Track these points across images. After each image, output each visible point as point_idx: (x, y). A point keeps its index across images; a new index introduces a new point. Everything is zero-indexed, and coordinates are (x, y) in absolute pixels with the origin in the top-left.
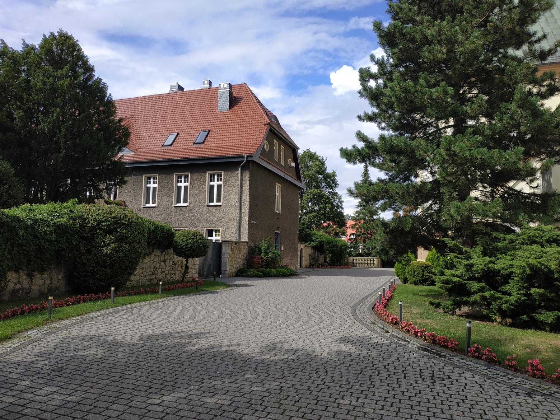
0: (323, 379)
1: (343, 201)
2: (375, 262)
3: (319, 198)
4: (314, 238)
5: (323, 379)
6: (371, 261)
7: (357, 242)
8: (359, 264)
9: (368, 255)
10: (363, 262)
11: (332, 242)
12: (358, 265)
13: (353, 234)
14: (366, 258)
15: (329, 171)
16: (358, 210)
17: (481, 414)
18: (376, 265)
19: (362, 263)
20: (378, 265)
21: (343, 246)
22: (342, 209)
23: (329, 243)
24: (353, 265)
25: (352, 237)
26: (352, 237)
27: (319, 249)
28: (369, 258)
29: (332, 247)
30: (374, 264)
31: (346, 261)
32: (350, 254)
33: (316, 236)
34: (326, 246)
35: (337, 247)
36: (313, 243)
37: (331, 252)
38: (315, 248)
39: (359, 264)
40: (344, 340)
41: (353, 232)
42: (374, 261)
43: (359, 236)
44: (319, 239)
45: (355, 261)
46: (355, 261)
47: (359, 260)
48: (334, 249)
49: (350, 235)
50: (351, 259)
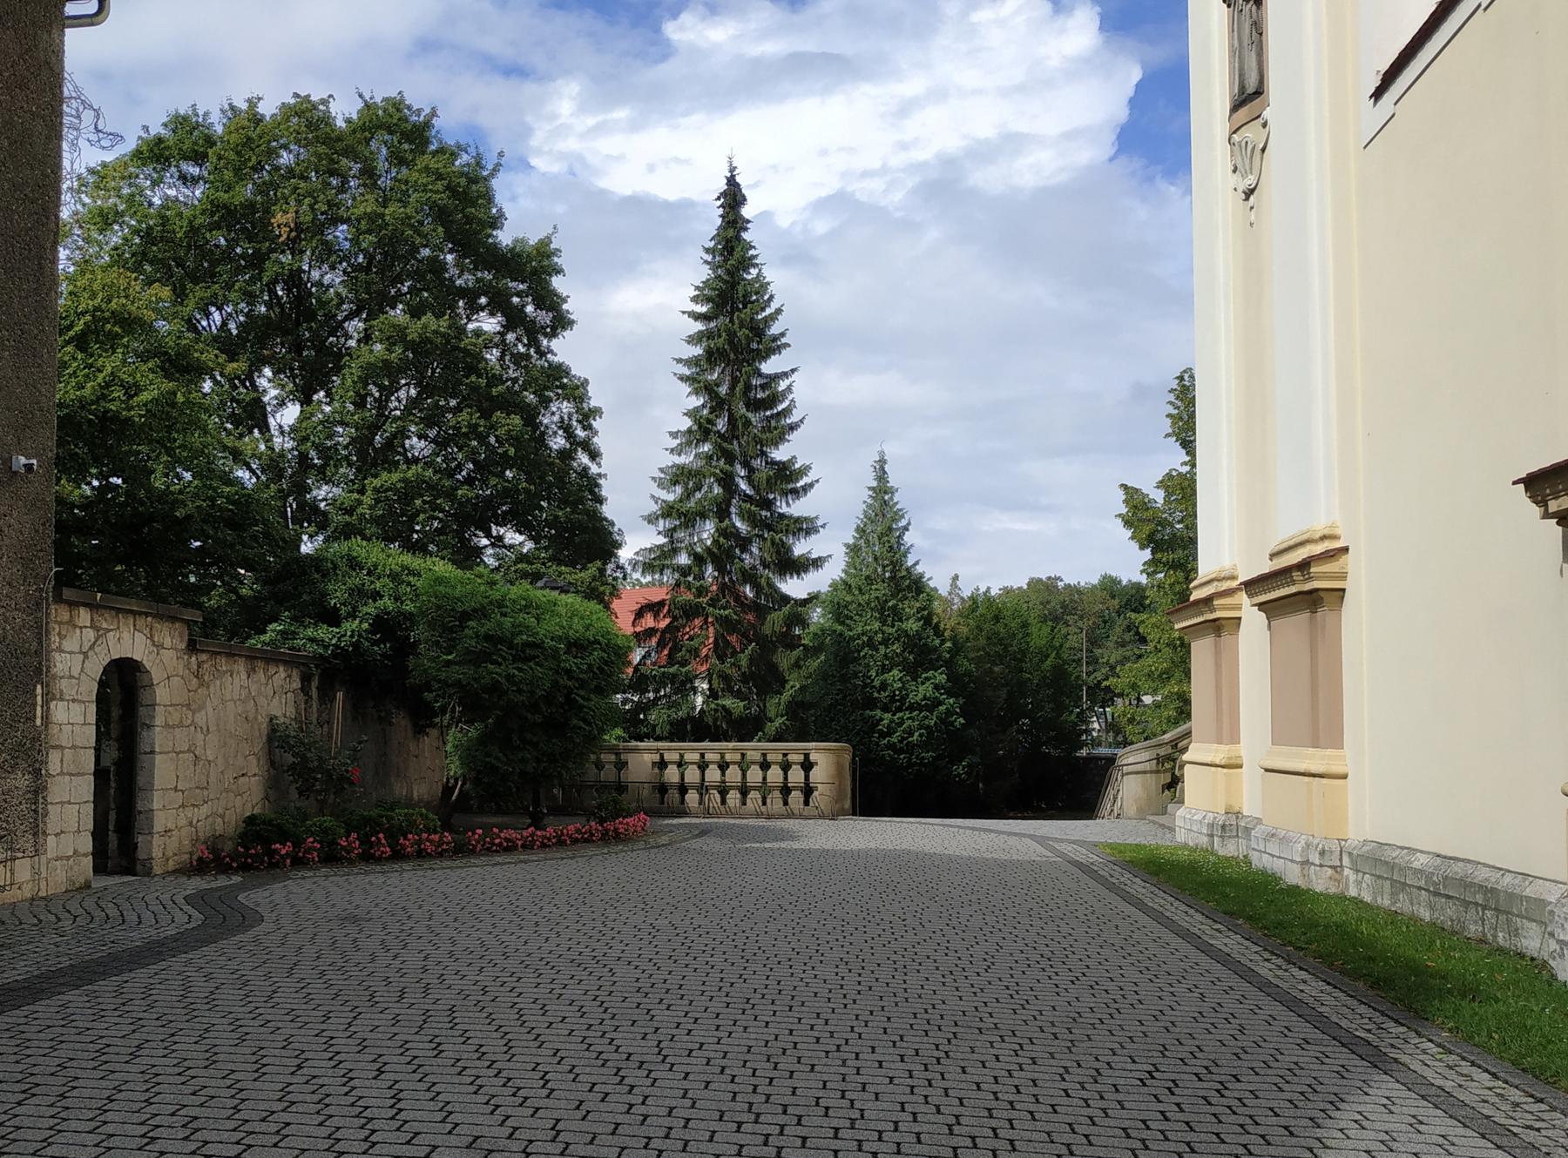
0: (620, 1083)
1: (596, 412)
2: (817, 775)
3: (447, 367)
4: (337, 594)
5: (620, 1083)
6: (765, 766)
7: (676, 648)
8: (702, 788)
9: (745, 728)
10: (733, 774)
11: (481, 613)
12: (692, 797)
13: (654, 608)
14: (730, 749)
15: (517, 227)
16: (686, 459)
17: (950, 1126)
18: (821, 796)
19: (764, 789)
20: (839, 798)
21: (578, 646)
22: (594, 455)
23: (452, 618)
24: (665, 799)
25: (649, 621)
26: (649, 621)
27: (375, 679)
28: (754, 749)
29: (476, 659)
30: (808, 791)
31: (608, 774)
32: (636, 727)
33: (354, 580)
34: (428, 659)
35: (529, 651)
36: (324, 632)
37: (473, 704)
38: (329, 674)
39: (702, 788)
40: (772, 297)
41: (658, 595)
42: (807, 766)
43: (691, 611)
44: (387, 603)
45: (672, 774)
46: (672, 774)
47: (689, 761)
48: (495, 671)
49: (639, 614)
50: (642, 759)
